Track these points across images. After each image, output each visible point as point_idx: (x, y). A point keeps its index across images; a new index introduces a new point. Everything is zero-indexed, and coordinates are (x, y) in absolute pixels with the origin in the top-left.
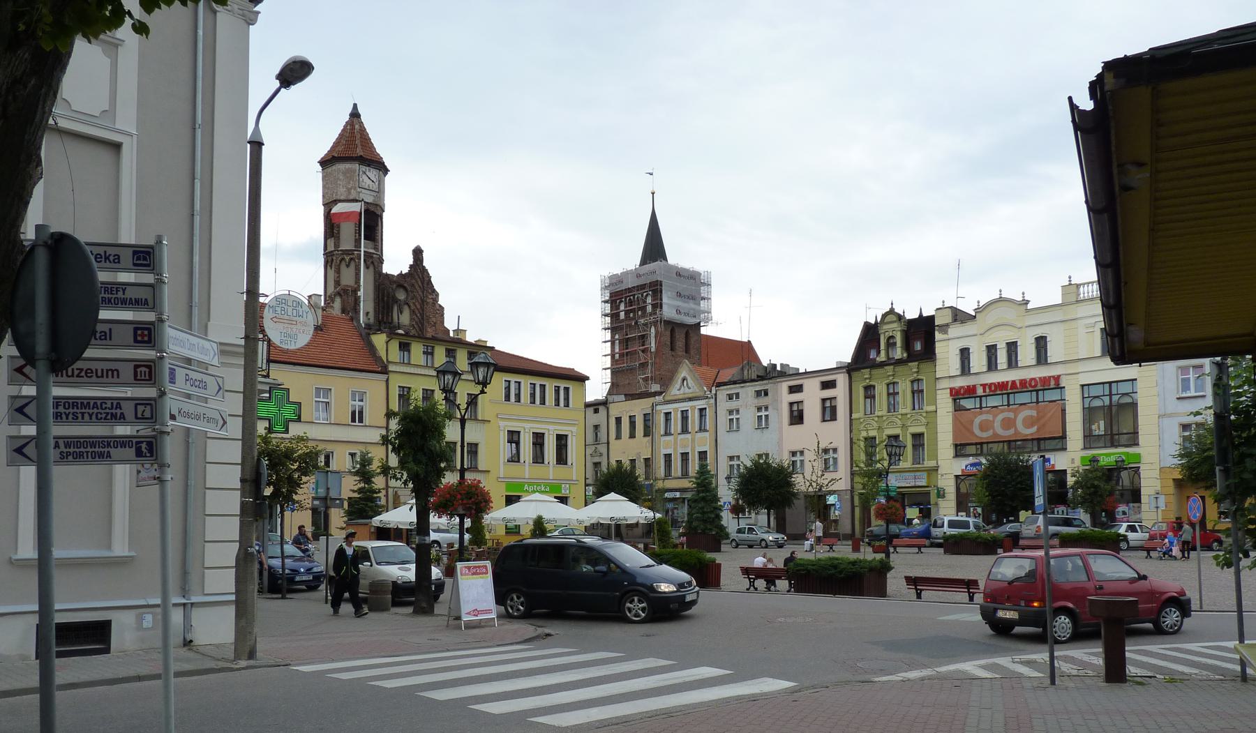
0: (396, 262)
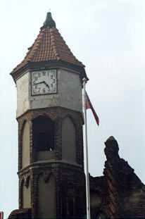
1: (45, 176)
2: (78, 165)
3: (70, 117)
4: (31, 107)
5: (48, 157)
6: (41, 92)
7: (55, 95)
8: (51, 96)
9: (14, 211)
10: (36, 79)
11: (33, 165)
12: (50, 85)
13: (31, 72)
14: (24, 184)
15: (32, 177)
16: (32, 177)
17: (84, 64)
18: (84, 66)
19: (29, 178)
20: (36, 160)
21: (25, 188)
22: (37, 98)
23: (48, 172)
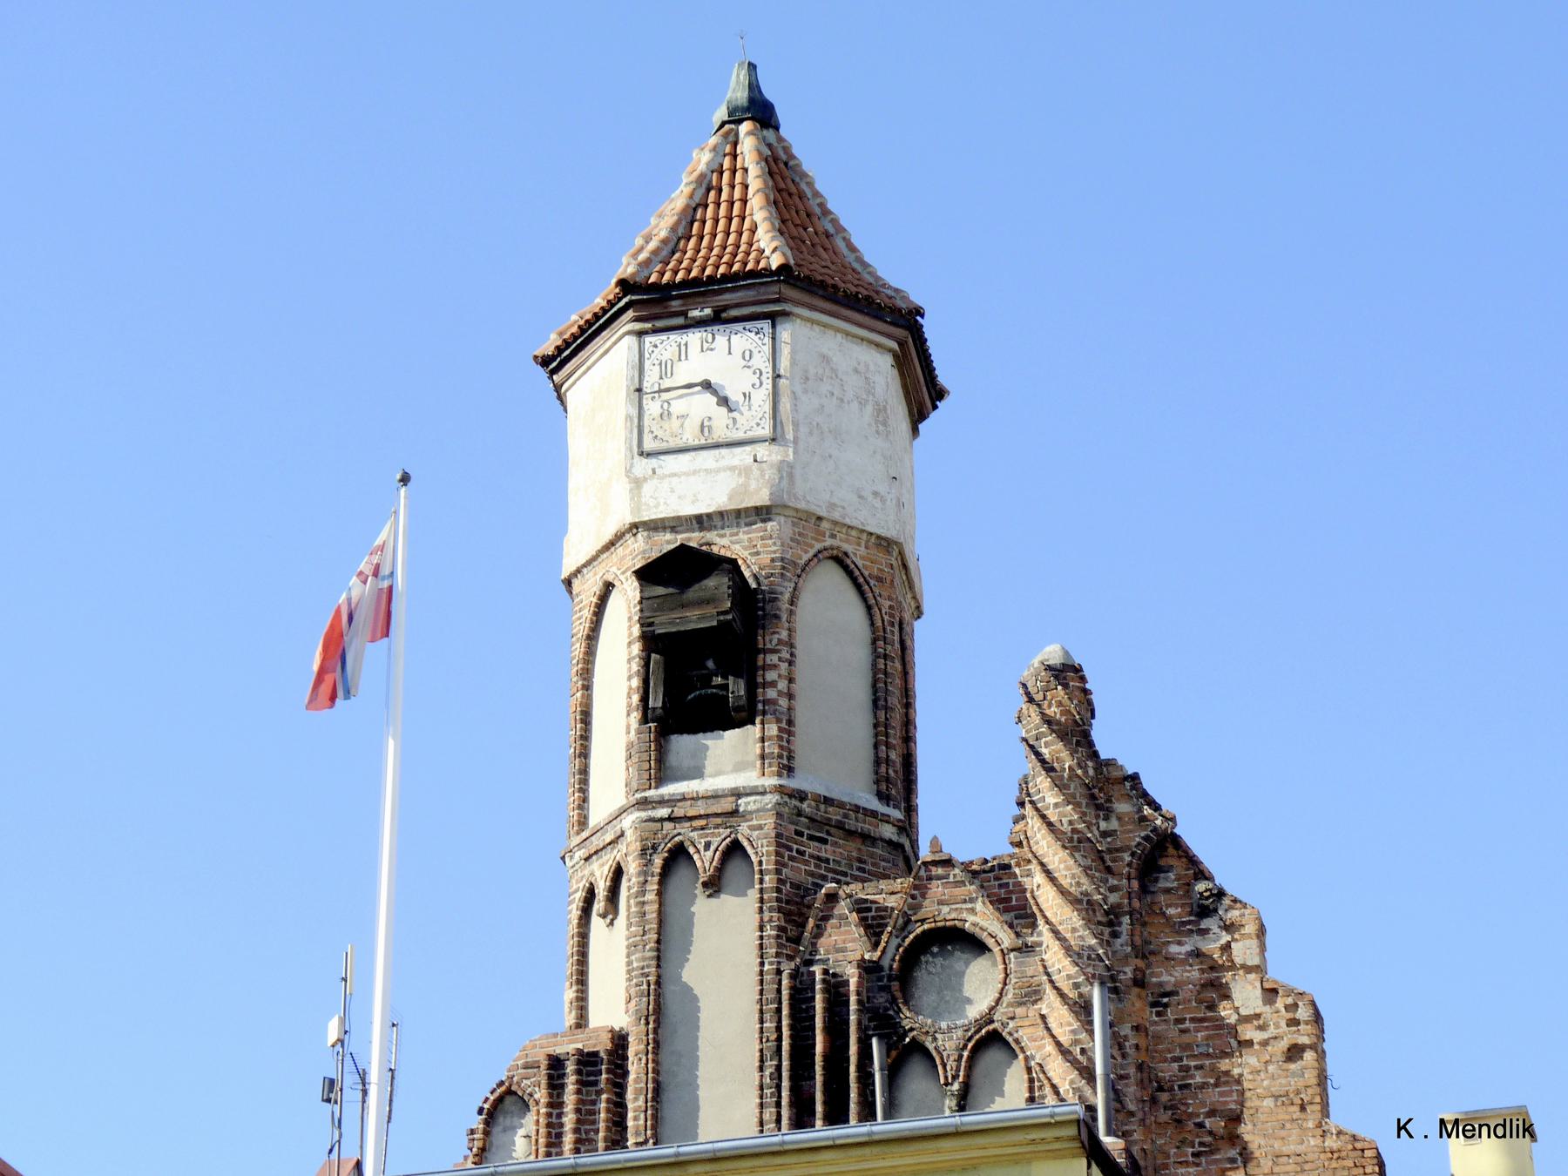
0: (977, 793)
1: (705, 861)
2: (882, 808)
3: (840, 560)
4: (637, 509)
5: (730, 762)
6: (690, 437)
7: (762, 451)
8: (742, 456)
9: (695, 999)
10: (666, 369)
11: (644, 803)
12: (734, 396)
13: (759, 651)
14: (599, 905)
15: (632, 867)
16: (632, 867)
17: (917, 298)
18: (919, 312)
19: (618, 873)
20: (660, 780)
21: (597, 923)
22: (671, 463)
23: (720, 838)
